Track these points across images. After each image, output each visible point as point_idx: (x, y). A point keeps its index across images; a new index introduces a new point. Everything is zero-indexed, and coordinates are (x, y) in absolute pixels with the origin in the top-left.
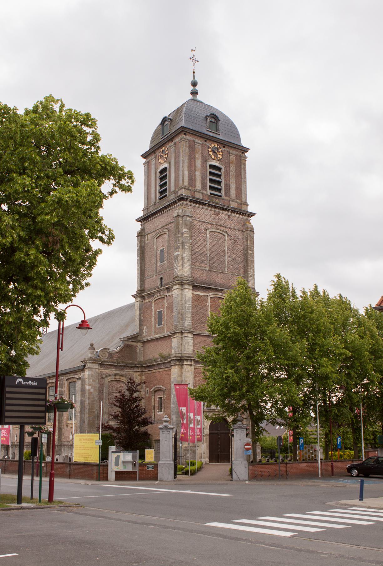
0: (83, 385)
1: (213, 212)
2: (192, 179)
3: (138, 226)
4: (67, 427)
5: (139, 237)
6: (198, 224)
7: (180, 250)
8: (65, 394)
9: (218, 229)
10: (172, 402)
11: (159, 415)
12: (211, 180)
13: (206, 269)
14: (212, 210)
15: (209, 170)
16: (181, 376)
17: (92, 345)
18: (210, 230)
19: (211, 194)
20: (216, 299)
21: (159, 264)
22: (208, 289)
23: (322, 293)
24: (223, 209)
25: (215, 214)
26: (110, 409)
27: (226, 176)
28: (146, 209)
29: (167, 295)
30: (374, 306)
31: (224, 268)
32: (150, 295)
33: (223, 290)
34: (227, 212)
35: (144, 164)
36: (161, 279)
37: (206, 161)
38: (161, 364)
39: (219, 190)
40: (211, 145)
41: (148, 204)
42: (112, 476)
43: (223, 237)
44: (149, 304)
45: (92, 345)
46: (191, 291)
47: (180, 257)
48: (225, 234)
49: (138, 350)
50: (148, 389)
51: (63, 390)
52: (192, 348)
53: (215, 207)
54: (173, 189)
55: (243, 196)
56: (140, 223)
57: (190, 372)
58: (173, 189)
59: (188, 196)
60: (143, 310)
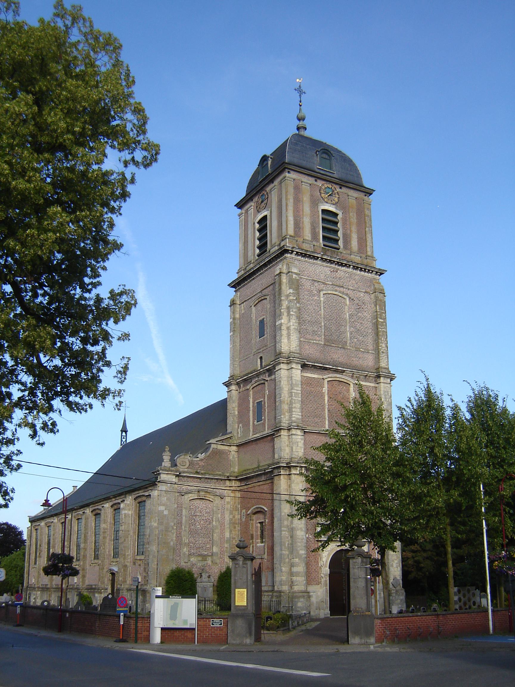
2: (298, 225)
6: (307, 284)
9: (336, 291)
13: (321, 342)
18: (324, 292)
23: (448, 412)
24: (342, 265)
26: (192, 539)
27: (344, 224)
33: (344, 371)
46: (299, 371)
48: (345, 297)
50: (244, 511)
52: (303, 451)
56: (234, 289)
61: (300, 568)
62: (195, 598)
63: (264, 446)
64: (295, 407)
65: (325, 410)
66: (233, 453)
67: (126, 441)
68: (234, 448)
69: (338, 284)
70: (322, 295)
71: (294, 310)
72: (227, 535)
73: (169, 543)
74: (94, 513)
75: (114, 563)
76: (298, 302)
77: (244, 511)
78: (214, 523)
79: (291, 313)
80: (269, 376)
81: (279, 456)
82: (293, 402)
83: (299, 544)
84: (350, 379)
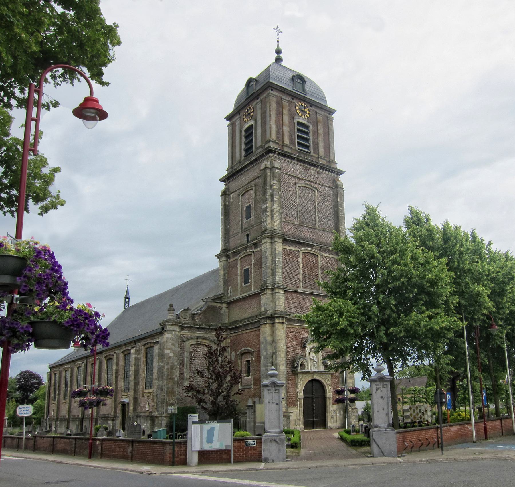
0: (162, 349)
2: (280, 133)
3: (222, 186)
4: (143, 396)
5: (223, 197)
8: (142, 362)
9: (308, 184)
11: (247, 380)
12: (298, 136)
13: (296, 223)
15: (296, 127)
17: (171, 306)
18: (299, 185)
19: (299, 149)
20: (307, 254)
21: (245, 221)
22: (299, 243)
24: (312, 165)
27: (314, 134)
28: (231, 167)
29: (255, 251)
30: (493, 248)
32: (235, 254)
33: (314, 245)
35: (228, 126)
36: (248, 236)
37: (293, 118)
38: (248, 324)
39: (307, 147)
40: (298, 103)
41: (232, 164)
42: (194, 458)
43: (313, 192)
44: (234, 262)
45: (171, 306)
47: (268, 210)
50: (234, 352)
51: (139, 356)
53: (304, 162)
54: (259, 143)
55: (331, 155)
57: (282, 331)
58: (259, 143)
59: (276, 149)
60: (229, 270)
62: (230, 422)
63: (254, 302)
66: (224, 308)
67: (129, 305)
68: (225, 305)
69: (309, 179)
70: (297, 187)
71: (277, 197)
73: (174, 378)
74: (107, 358)
75: (125, 397)
77: (234, 352)
79: (275, 199)
80: (255, 248)
81: (265, 309)
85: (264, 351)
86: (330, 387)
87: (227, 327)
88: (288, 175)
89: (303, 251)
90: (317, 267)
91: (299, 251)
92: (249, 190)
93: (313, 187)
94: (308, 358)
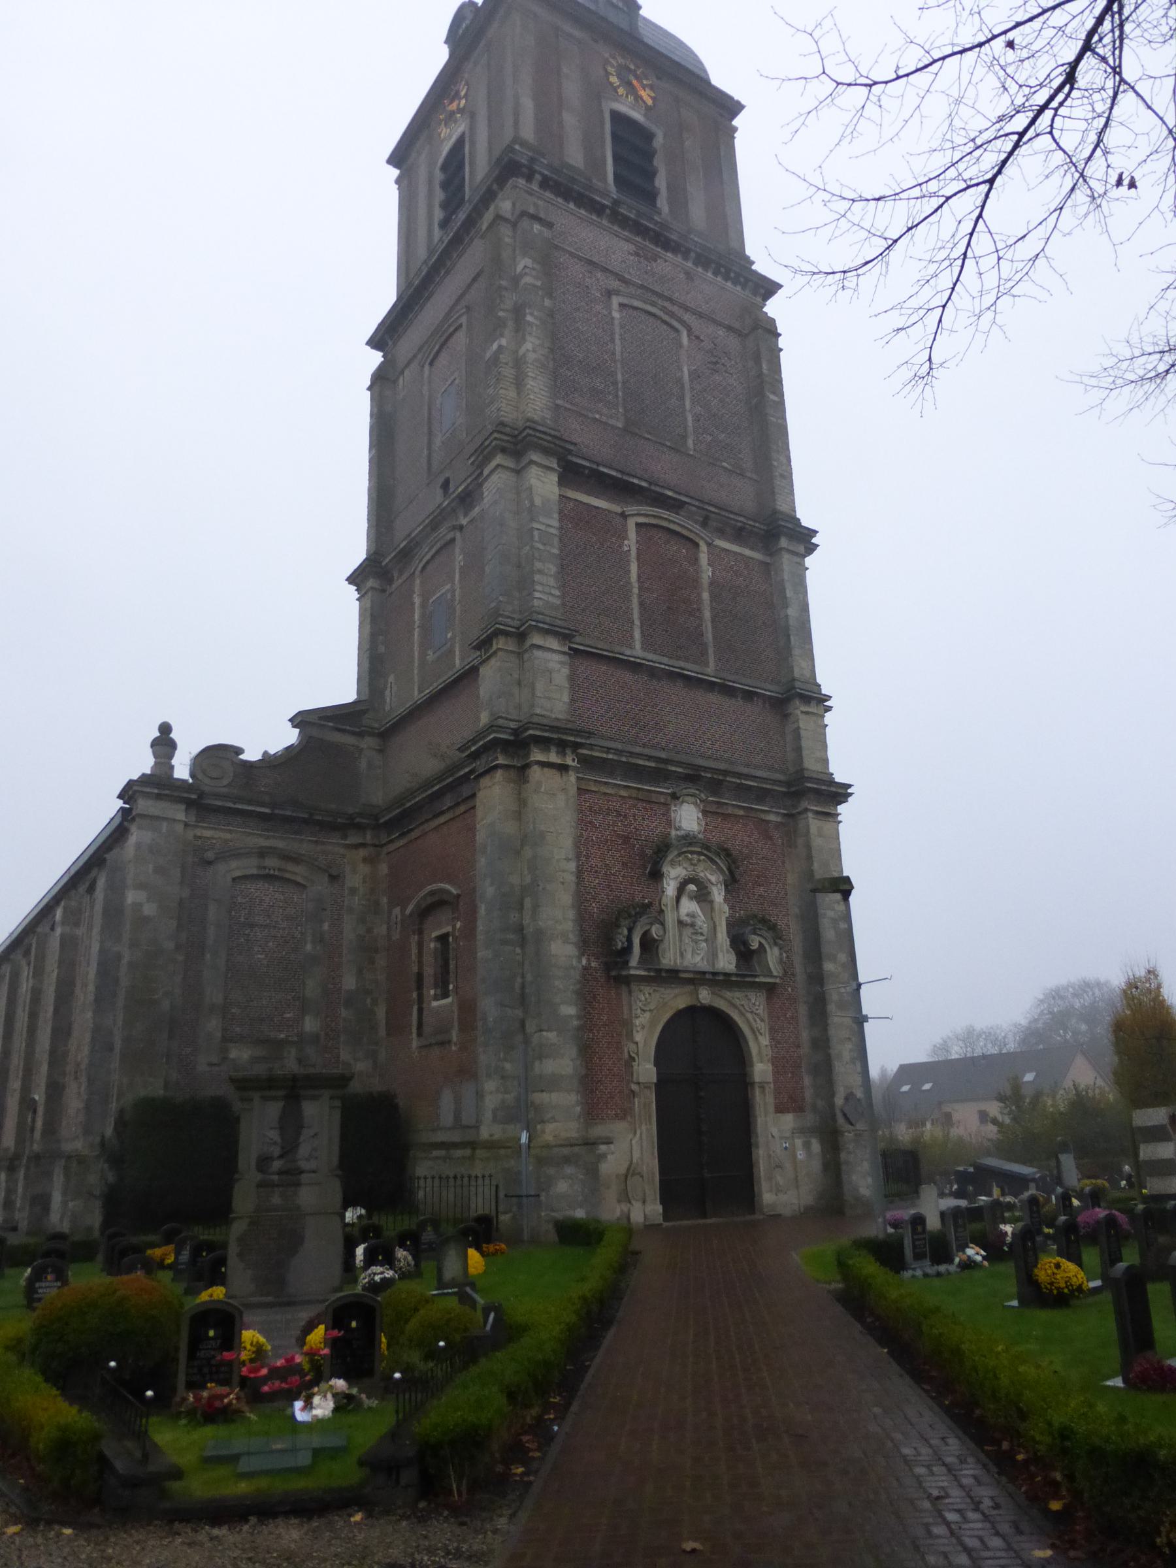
1: (632, 248)
7: (507, 332)
9: (653, 304)
10: (480, 937)
13: (612, 422)
14: (627, 240)
16: (519, 816)
25: (637, 255)
31: (684, 438)
34: (679, 259)
43: (673, 335)
46: (554, 478)
49: (363, 765)
50: (397, 911)
51: (79, 932)
52: (566, 698)
61: (563, 1063)
64: (540, 572)
65: (629, 601)
69: (657, 289)
70: (615, 305)
72: (349, 982)
76: (550, 295)
78: (309, 947)
79: (529, 318)
82: (536, 555)
83: (557, 983)
84: (697, 528)
85: (488, 881)
86: (765, 1041)
87: (376, 818)
88: (580, 259)
89: (641, 520)
90: (695, 583)
91: (624, 516)
92: (451, 335)
93: (672, 315)
94: (670, 918)
